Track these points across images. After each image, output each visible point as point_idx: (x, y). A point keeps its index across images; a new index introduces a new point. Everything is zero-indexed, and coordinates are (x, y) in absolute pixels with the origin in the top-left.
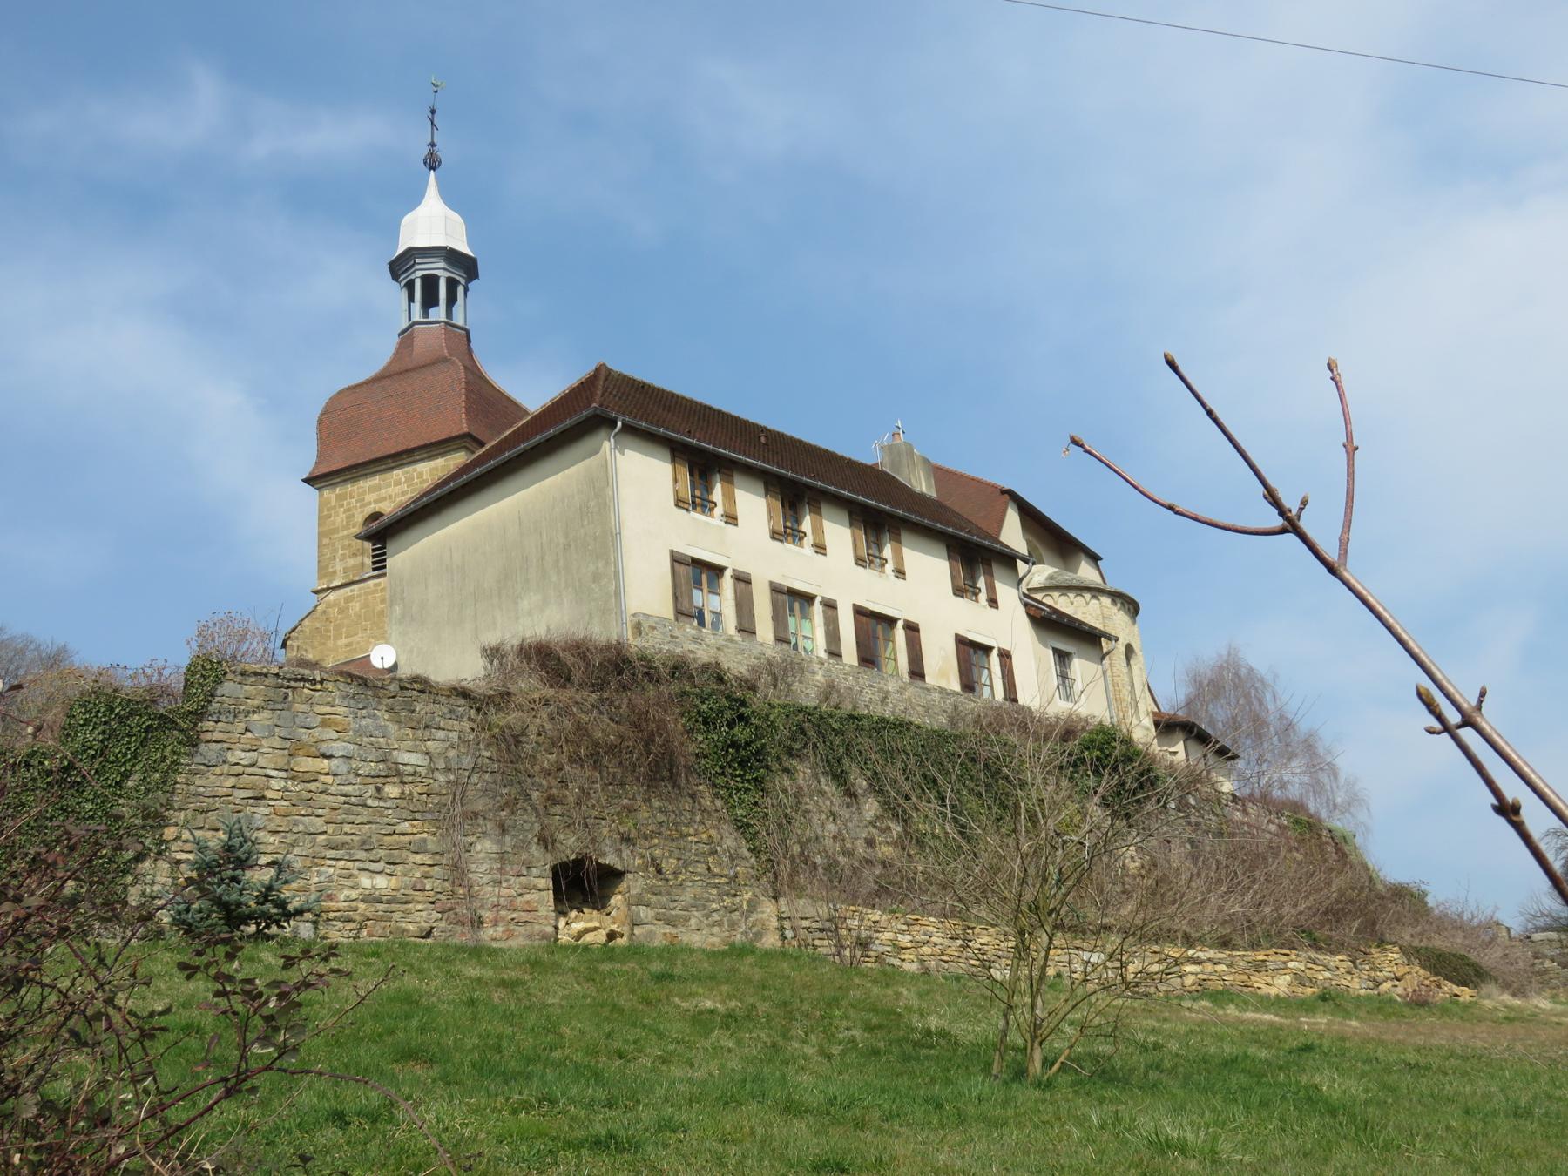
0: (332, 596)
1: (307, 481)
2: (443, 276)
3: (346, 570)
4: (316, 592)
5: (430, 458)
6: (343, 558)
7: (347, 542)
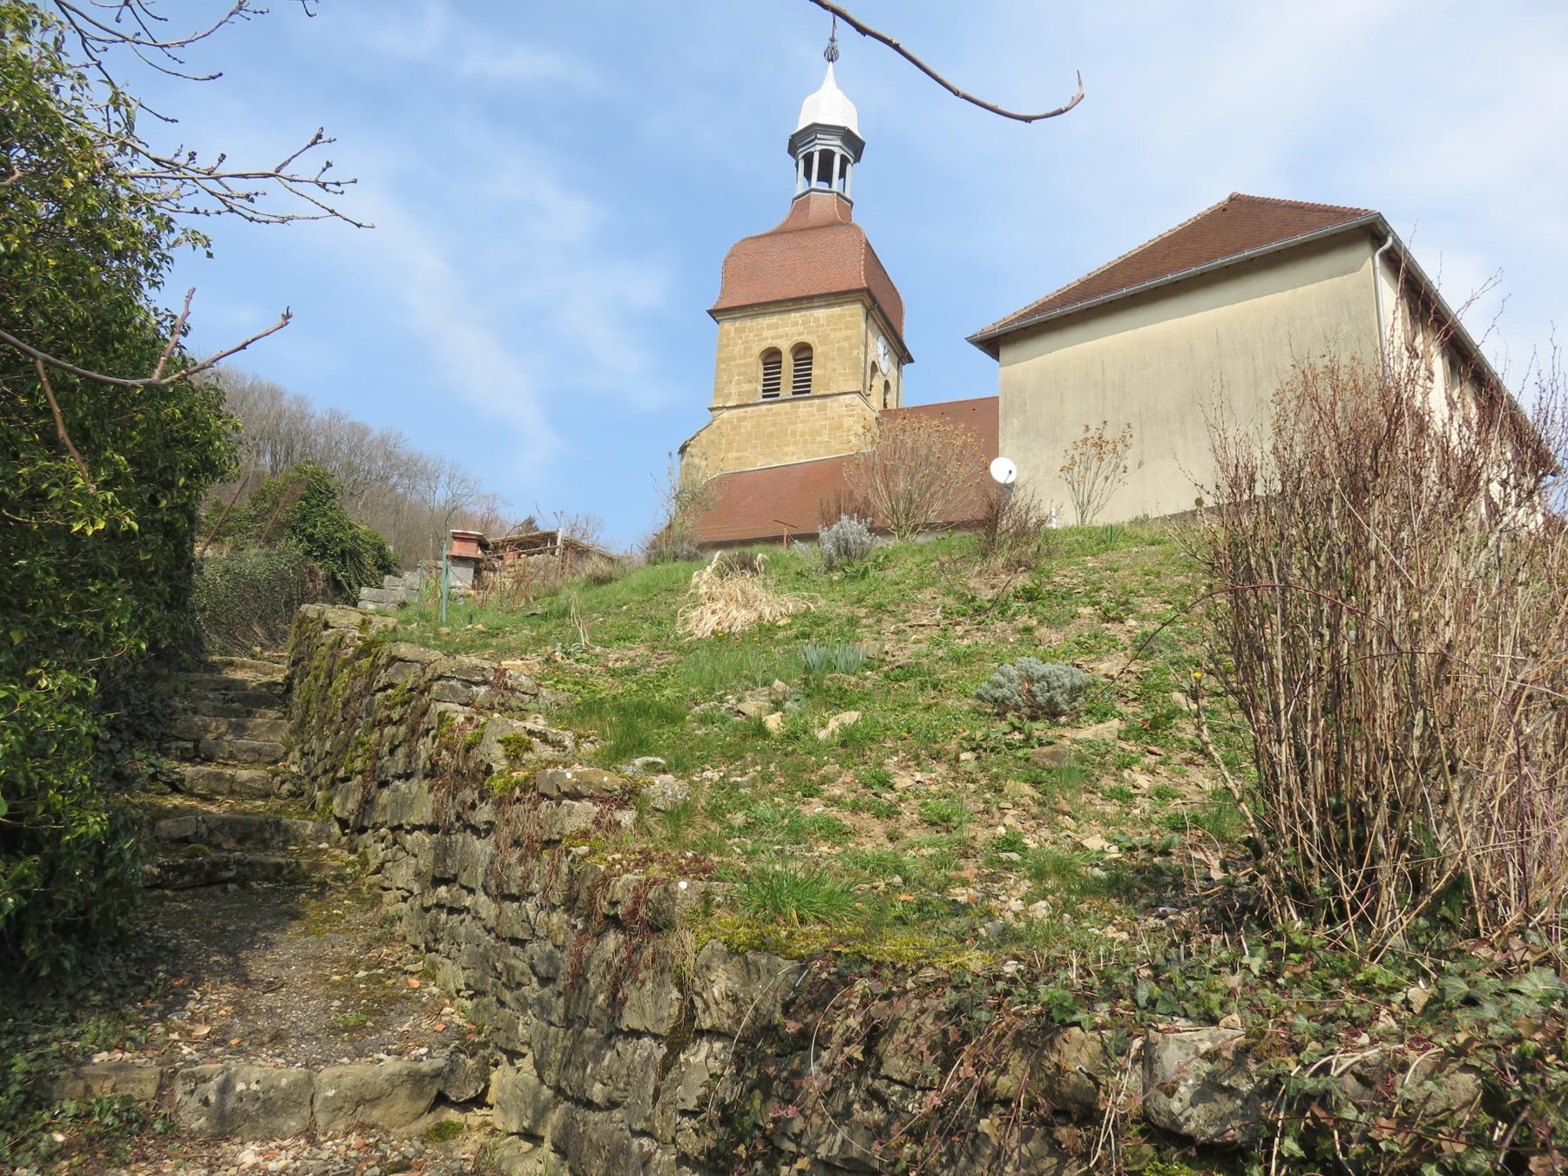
0: (726, 414)
1: (710, 312)
2: (839, 152)
3: (740, 394)
4: (711, 409)
5: (827, 306)
6: (739, 383)
7: (743, 370)
